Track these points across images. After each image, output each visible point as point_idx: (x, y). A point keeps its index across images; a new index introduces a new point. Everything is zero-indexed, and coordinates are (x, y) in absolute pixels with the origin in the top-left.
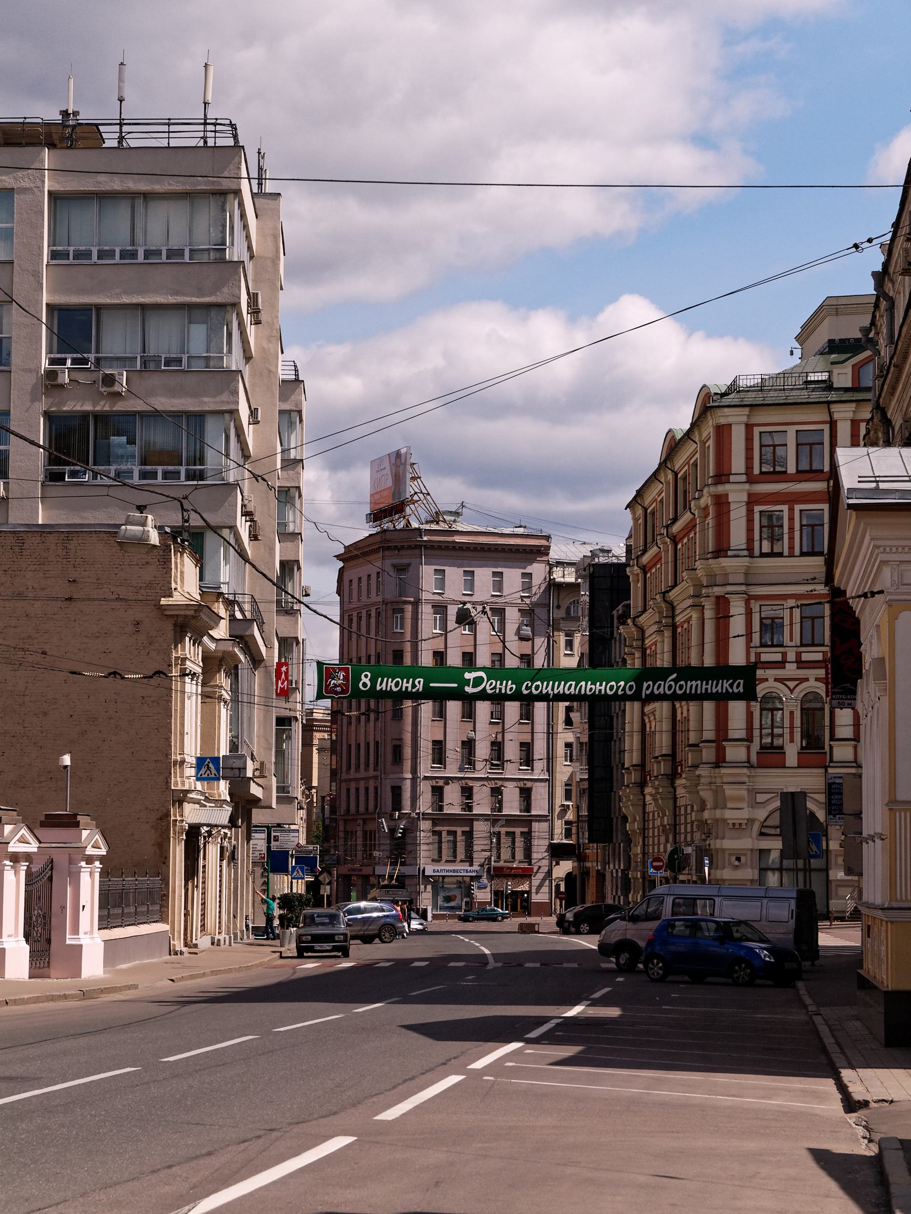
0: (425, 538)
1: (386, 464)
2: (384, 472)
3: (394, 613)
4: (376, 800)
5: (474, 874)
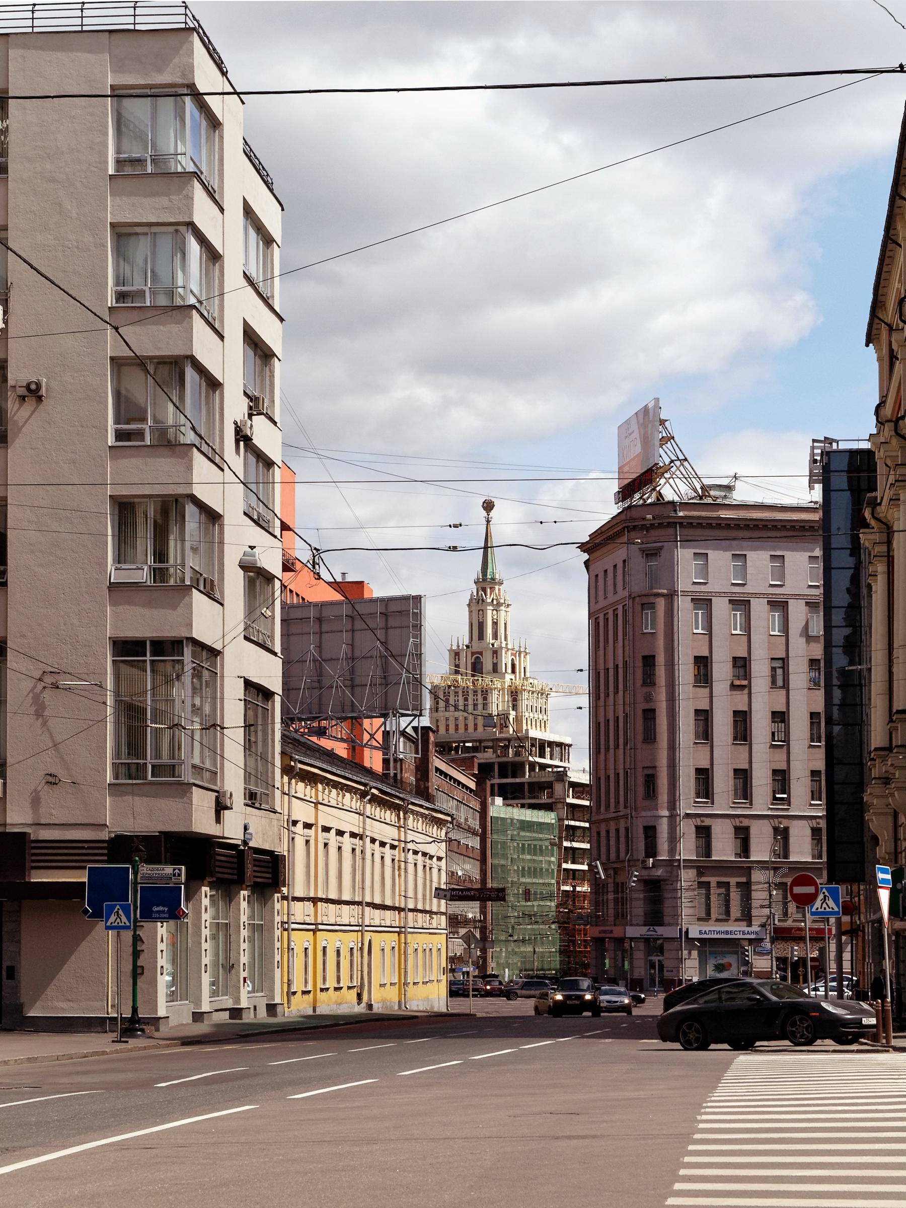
0: (681, 514)
1: (634, 427)
2: (632, 437)
3: (643, 609)
4: (627, 845)
5: (753, 936)
